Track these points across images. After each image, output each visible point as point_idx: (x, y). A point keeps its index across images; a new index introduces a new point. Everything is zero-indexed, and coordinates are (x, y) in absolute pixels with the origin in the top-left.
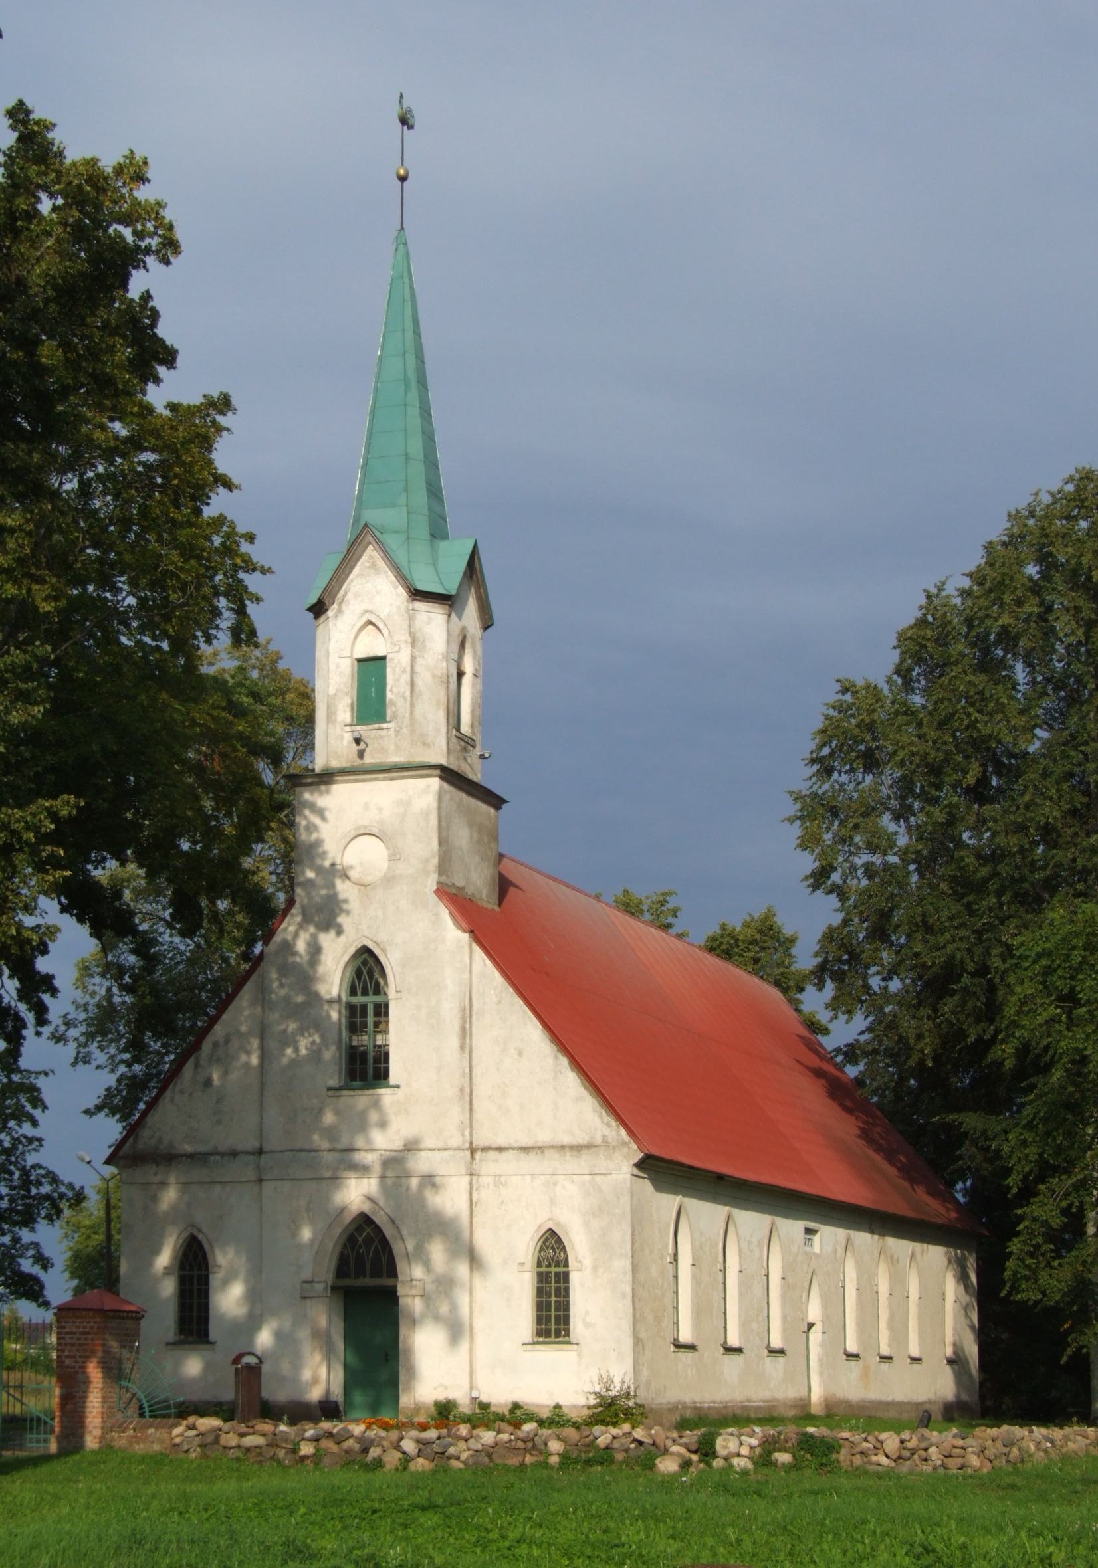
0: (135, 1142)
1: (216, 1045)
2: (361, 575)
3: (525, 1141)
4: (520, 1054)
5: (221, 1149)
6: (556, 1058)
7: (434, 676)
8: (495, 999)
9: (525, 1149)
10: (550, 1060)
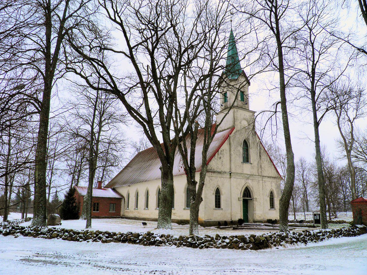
1: (221, 151)
3: (268, 176)
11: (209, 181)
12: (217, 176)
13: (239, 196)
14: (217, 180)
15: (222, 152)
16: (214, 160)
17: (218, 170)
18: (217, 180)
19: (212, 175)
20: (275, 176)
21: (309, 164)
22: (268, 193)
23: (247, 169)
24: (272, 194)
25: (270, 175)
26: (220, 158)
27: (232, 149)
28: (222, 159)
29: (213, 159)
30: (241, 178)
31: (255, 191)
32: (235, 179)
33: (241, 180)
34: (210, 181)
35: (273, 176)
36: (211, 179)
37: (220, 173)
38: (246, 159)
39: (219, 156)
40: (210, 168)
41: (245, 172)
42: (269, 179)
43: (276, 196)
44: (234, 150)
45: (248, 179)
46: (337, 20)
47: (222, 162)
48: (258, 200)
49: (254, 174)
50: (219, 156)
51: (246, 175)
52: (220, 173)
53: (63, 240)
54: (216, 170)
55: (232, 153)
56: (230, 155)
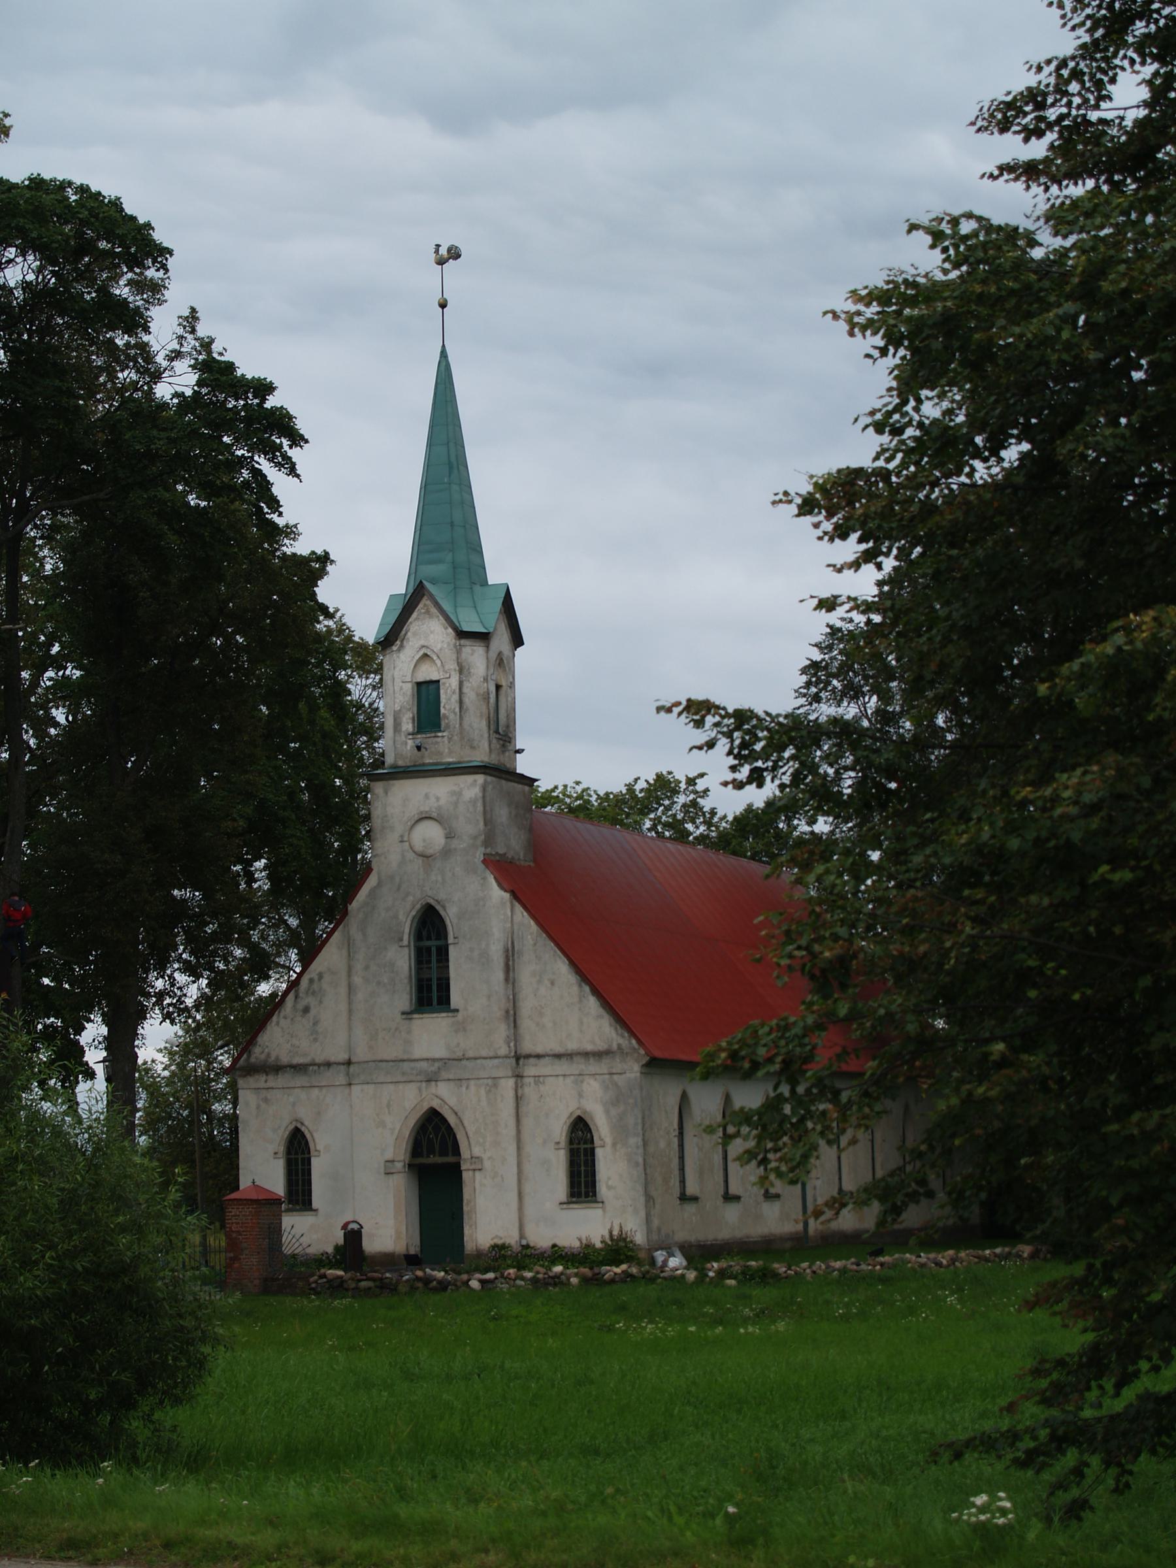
0: (249, 1056)
1: (311, 981)
2: (417, 619)
3: (559, 1049)
4: (552, 983)
5: (317, 1061)
6: (580, 986)
7: (478, 695)
8: (532, 942)
9: (558, 1056)
10: (575, 989)
11: (258, 1107)
12: (292, 1084)
13: (389, 1155)
14: (291, 1099)
15: (315, 986)
16: (278, 1023)
17: (297, 1060)
18: (291, 1099)
19: (269, 1084)
20: (601, 1046)
21: (999, 1457)
22: (559, 1129)
23: (431, 1036)
24: (580, 1129)
25: (572, 1046)
26: (306, 1010)
27: (358, 966)
28: (313, 1012)
29: (275, 1018)
30: (400, 1078)
31: (471, 1129)
32: (370, 1089)
33: (401, 1086)
34: (263, 1105)
35: (589, 1047)
36: (266, 1100)
37: (299, 1069)
38: (431, 992)
39: (301, 1004)
40: (263, 1057)
41: (418, 1053)
42: (562, 1067)
43: (608, 1140)
44: (367, 968)
45: (431, 1079)
46: (816, 645)
47: (315, 1024)
48: (487, 1164)
49: (471, 1054)
50: (301, 1004)
51: (424, 1065)
52: (299, 1069)
53: (678, 700)
54: (285, 1060)
55: (357, 980)
56: (351, 989)
